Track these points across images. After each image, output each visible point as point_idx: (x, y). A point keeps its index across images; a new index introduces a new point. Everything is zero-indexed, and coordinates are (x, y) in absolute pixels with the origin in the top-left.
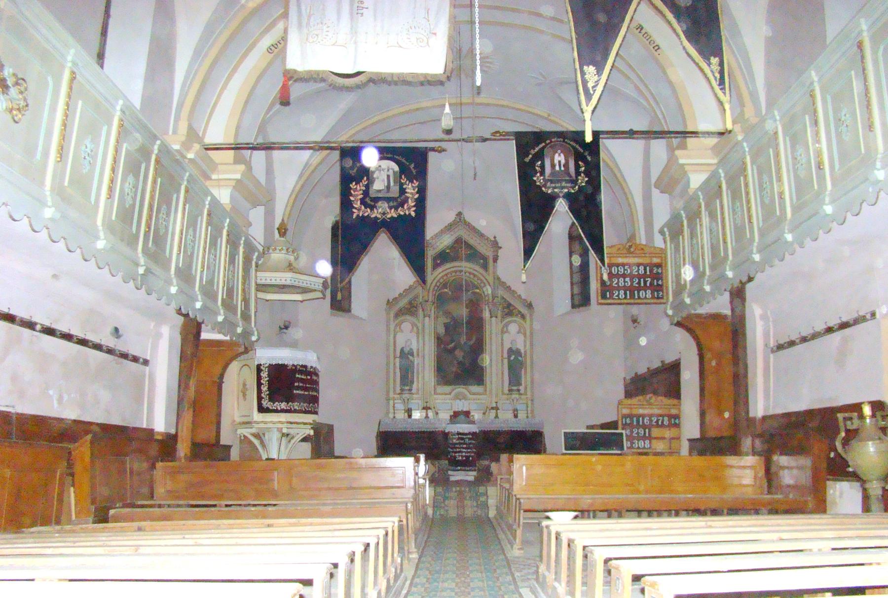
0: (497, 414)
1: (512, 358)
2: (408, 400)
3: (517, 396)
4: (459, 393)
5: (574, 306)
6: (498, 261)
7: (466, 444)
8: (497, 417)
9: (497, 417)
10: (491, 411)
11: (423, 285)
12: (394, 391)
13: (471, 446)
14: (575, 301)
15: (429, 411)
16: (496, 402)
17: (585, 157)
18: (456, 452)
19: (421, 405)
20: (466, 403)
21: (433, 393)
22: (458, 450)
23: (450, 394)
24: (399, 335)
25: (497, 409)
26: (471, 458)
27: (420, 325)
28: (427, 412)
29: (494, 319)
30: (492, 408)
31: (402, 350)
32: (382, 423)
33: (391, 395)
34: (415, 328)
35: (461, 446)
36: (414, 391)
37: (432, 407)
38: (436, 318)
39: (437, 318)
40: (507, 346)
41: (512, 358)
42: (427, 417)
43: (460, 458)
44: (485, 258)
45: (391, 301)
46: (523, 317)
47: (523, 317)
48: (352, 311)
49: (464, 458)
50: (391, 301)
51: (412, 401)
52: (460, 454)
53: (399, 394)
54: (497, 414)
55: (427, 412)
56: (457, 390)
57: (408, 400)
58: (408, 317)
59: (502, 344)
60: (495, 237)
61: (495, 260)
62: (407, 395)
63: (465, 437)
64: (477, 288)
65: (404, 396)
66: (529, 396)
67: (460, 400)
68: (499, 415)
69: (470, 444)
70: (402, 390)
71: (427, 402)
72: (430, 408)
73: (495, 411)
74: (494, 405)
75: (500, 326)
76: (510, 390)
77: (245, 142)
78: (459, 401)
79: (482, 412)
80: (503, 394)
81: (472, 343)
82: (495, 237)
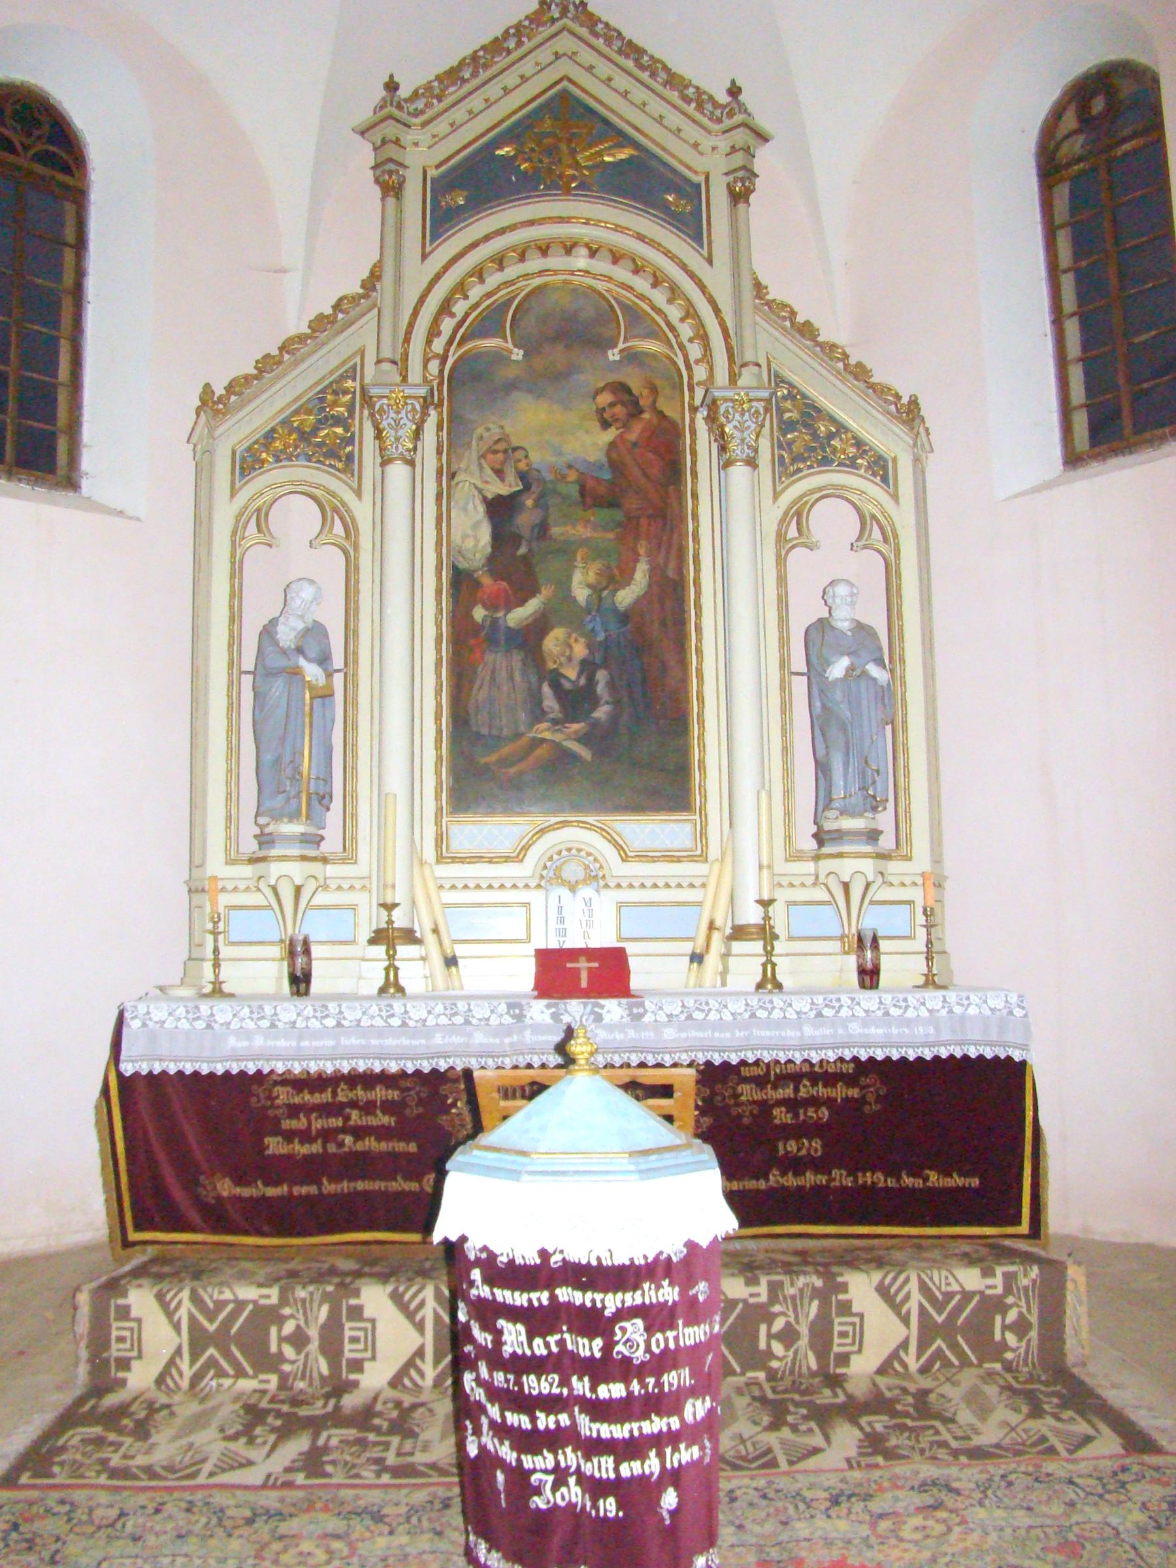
0: (769, 963)
1: (838, 669)
2: (298, 890)
3: (867, 866)
4: (572, 851)
5: (1073, 459)
6: (753, 198)
7: (625, 1370)
8: (769, 982)
9: (769, 982)
10: (737, 947)
11: (626, 1075)
12: (232, 840)
13: (672, 1379)
14: (1077, 441)
15: (404, 951)
16: (765, 904)
17: (324, 1327)
18: (530, 1442)
19: (369, 920)
20: (605, 903)
21: (430, 853)
22: (545, 1421)
23: (518, 857)
24: (256, 559)
25: (766, 933)
26: (670, 1499)
27: (362, 511)
28: (391, 957)
29: (739, 472)
30: (739, 933)
31: (268, 632)
32: (133, 1025)
33: (216, 865)
34: (339, 528)
35: (581, 1386)
36: (332, 843)
37: (423, 928)
38: (448, 475)
39: (452, 476)
40: (804, 614)
41: (838, 669)
42: (392, 987)
43: (573, 1493)
44: (693, 192)
45: (219, 391)
46: (881, 469)
47: (881, 469)
48: (85, 483)
49: (609, 1506)
50: (219, 391)
51: (321, 898)
52: (570, 1457)
53: (253, 860)
54: (769, 963)
55: (391, 957)
56: (551, 839)
57: (298, 890)
58: (302, 472)
59: (783, 603)
60: (734, 91)
61: (739, 196)
62: (297, 871)
63: (611, 1302)
64: (654, 334)
65: (275, 870)
66: (922, 860)
67: (573, 888)
68: (784, 973)
69: (663, 1362)
70: (265, 840)
71: (390, 907)
72: (410, 937)
73: (757, 946)
74: (752, 915)
75: (773, 514)
76: (820, 838)
77: (229, 476)
78: (564, 892)
79: (688, 947)
80: (796, 856)
81: (625, 597)
82: (734, 91)
